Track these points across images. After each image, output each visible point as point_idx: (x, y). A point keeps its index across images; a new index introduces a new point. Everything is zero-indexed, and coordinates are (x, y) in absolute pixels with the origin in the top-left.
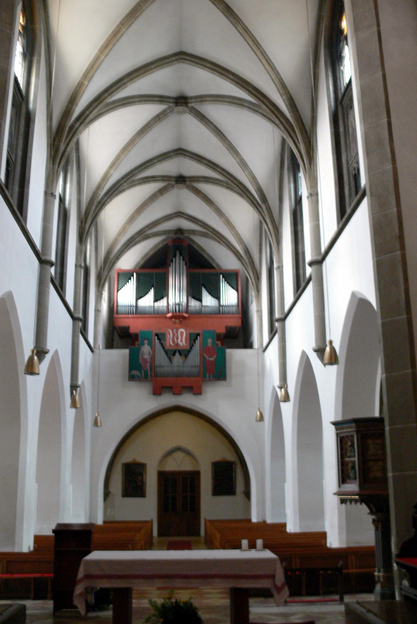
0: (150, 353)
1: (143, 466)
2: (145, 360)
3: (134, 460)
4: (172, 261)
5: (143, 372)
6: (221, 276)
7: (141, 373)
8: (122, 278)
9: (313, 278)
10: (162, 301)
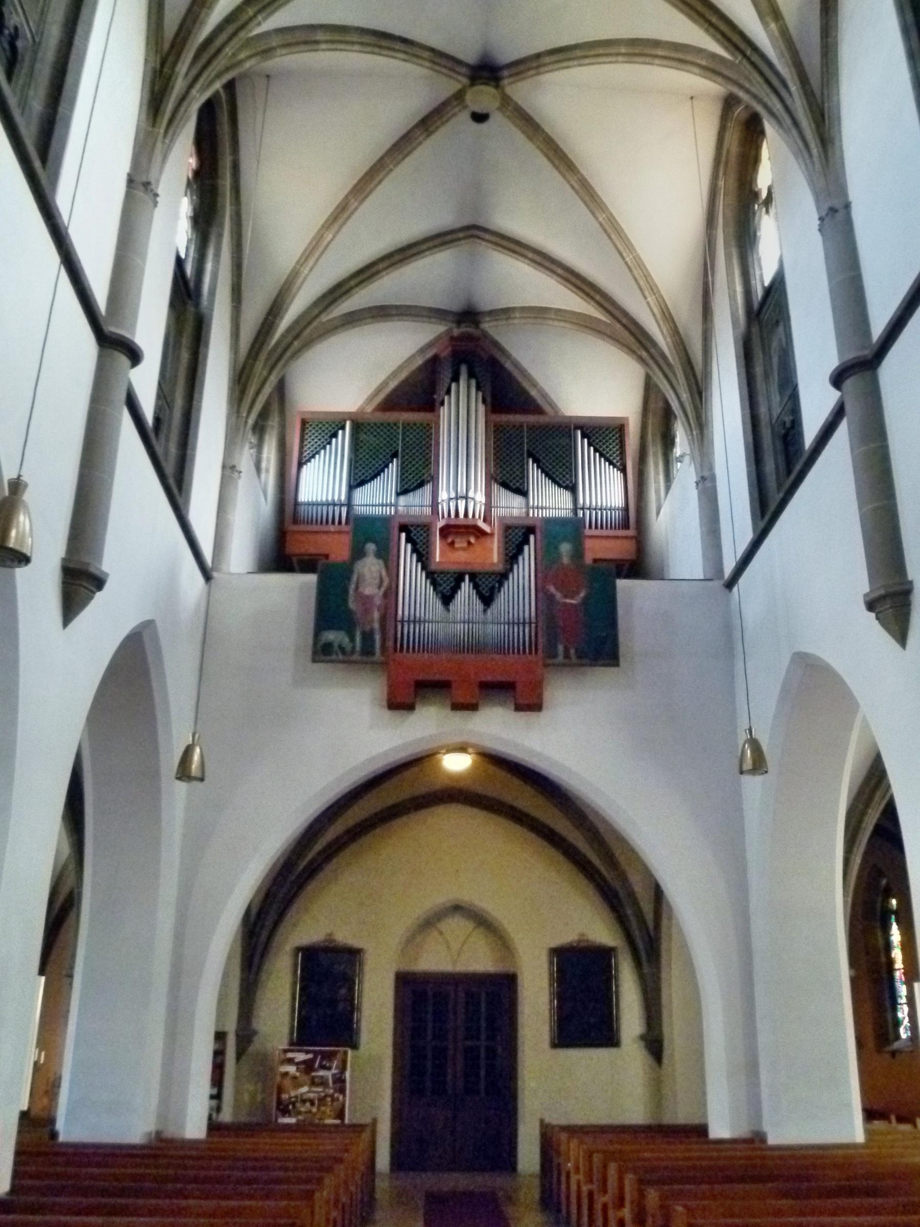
0: (381, 581)
1: (353, 955)
2: (366, 601)
3: (330, 938)
4: (448, 392)
5: (358, 639)
6: (579, 433)
7: (352, 639)
8: (313, 434)
9: (848, 408)
10: (419, 492)
